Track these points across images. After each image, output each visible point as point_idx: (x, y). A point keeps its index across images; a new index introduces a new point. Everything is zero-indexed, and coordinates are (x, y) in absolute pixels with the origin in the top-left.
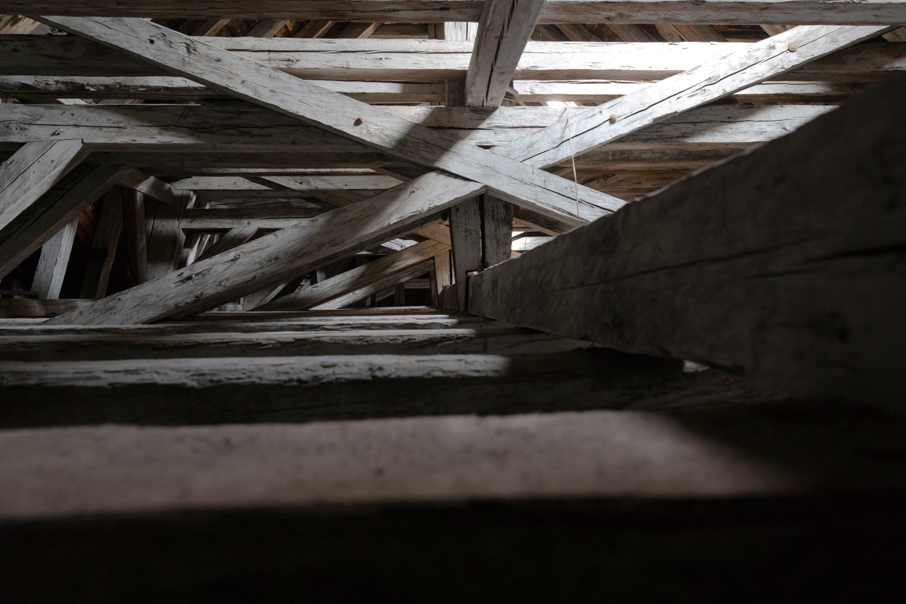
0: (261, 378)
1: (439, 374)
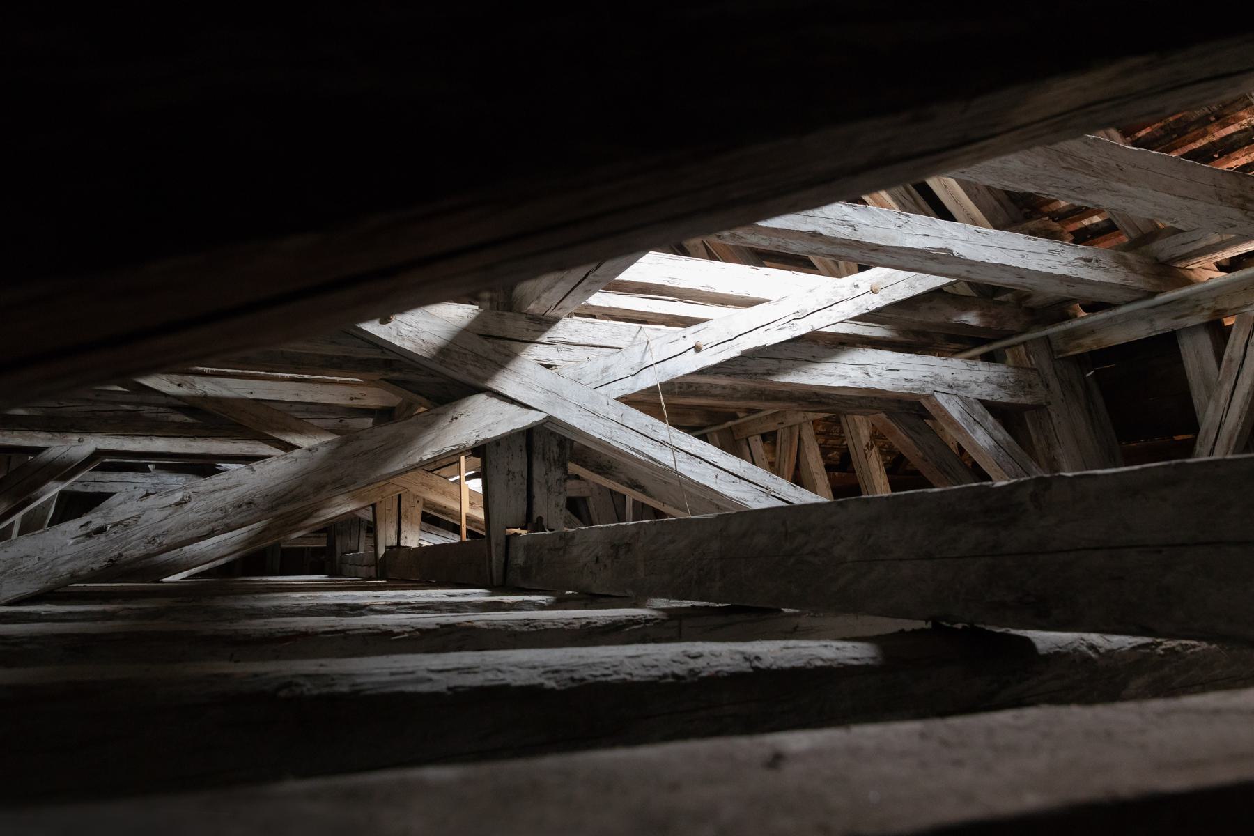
1: (819, 663)
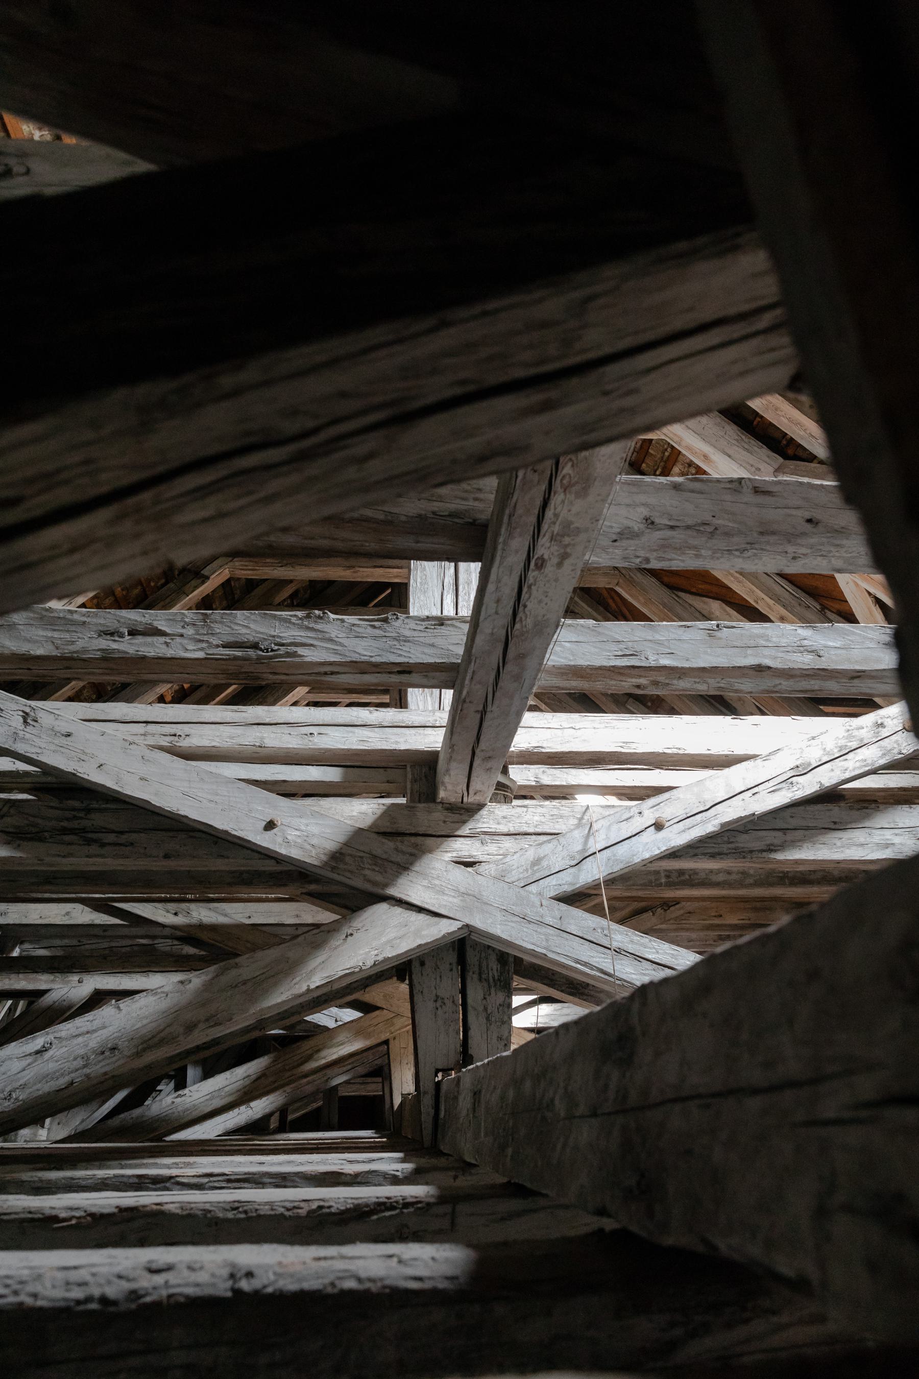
0: (35, 1296)
1: (350, 1284)
